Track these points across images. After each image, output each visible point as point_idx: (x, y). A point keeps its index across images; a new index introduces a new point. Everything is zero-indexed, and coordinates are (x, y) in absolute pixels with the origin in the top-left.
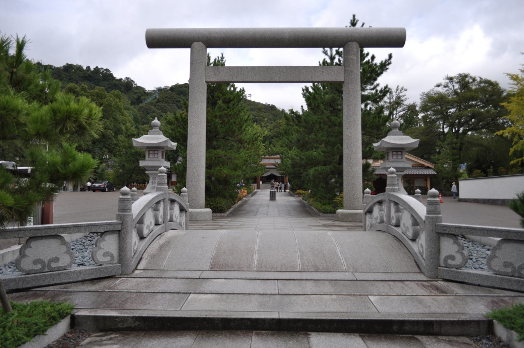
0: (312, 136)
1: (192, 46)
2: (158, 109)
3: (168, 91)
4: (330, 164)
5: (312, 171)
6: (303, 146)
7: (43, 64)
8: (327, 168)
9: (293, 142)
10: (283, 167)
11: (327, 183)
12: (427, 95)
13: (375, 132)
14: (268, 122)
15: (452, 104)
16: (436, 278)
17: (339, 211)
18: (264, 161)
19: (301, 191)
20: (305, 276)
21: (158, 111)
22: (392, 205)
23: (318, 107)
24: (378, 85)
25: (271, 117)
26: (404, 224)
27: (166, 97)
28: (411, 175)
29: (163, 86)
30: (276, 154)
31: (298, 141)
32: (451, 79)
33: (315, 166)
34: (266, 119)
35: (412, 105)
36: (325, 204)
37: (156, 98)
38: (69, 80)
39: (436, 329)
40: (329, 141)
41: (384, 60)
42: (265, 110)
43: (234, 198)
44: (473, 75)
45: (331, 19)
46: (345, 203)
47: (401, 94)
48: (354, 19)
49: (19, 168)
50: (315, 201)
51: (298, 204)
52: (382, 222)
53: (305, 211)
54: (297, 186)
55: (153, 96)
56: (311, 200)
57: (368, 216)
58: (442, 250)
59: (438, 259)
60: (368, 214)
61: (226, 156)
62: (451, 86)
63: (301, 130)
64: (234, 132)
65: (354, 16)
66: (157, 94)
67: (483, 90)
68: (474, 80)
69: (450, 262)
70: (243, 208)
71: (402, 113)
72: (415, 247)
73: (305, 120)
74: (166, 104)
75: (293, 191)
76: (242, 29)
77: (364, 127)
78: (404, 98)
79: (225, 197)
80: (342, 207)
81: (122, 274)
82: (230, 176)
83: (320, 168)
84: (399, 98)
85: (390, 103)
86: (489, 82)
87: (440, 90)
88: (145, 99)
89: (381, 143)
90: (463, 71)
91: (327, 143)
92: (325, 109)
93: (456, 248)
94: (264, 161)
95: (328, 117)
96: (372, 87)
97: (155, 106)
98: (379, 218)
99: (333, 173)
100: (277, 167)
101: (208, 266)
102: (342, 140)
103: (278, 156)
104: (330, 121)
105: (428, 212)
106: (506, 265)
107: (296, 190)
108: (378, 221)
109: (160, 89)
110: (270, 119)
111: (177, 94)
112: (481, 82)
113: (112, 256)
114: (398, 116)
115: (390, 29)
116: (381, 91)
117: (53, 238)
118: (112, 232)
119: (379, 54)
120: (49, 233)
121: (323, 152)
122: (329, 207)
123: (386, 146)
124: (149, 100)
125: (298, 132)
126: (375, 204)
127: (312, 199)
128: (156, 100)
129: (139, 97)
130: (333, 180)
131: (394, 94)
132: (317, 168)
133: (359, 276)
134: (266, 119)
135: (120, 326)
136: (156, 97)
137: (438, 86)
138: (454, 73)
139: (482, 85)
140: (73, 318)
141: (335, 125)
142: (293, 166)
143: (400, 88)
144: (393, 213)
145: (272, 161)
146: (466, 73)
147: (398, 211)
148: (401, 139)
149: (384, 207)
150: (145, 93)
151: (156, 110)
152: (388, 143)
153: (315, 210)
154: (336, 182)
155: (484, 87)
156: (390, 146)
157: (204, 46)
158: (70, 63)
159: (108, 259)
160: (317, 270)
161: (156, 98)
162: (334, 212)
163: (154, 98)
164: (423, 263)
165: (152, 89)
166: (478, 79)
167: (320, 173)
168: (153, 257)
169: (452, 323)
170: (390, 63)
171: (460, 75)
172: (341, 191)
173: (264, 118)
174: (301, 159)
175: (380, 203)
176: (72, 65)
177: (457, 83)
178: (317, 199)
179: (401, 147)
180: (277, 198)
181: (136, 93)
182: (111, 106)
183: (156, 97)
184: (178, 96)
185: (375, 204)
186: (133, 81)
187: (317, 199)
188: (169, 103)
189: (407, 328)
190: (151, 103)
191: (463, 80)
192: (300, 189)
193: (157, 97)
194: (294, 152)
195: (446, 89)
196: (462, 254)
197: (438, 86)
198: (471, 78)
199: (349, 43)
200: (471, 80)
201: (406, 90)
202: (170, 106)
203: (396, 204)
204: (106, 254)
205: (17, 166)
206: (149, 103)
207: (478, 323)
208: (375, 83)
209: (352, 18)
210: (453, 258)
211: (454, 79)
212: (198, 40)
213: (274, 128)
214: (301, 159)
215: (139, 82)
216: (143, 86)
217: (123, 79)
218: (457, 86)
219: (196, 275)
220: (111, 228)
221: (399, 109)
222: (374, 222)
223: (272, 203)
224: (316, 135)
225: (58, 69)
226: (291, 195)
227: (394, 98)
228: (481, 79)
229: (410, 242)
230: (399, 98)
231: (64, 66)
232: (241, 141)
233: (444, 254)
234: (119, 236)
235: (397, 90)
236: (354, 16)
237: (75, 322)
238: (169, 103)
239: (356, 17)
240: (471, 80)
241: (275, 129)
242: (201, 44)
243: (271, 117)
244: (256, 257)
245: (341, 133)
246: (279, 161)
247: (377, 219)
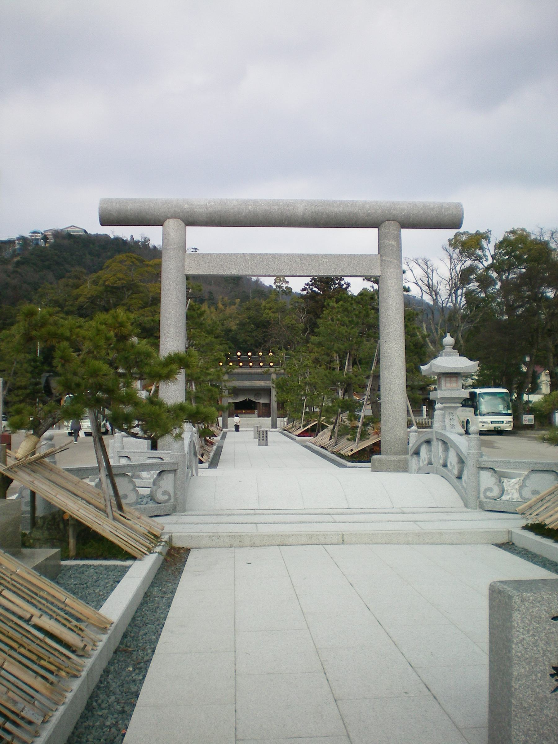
1: (166, 223)
22: (440, 443)
26: (451, 463)
58: (481, 484)
59: (479, 492)
60: (415, 456)
69: (489, 494)
89: (431, 366)
98: (427, 459)
106: (535, 492)
108: (426, 462)
113: (169, 495)
117: (122, 477)
118: (170, 471)
139: (212, 203)
152: (440, 366)
157: (183, 224)
159: (166, 497)
179: (456, 371)
203: (444, 443)
204: (165, 493)
210: (490, 489)
219: (252, 512)
222: (421, 465)
234: (175, 476)
247: (425, 460)
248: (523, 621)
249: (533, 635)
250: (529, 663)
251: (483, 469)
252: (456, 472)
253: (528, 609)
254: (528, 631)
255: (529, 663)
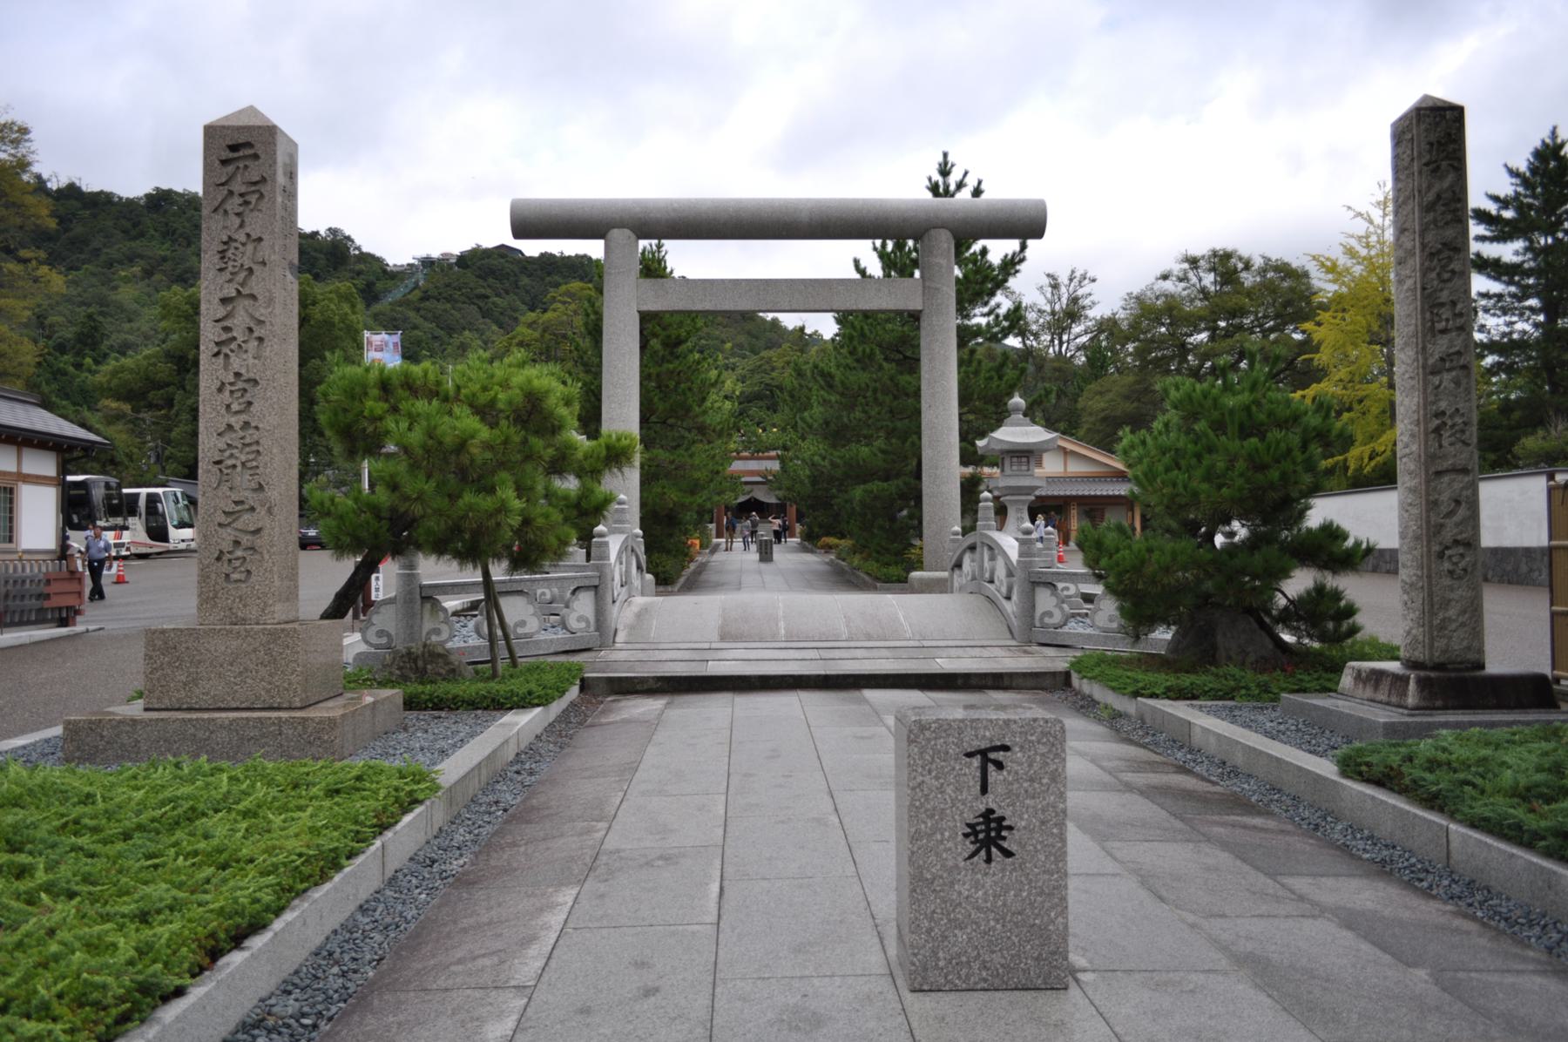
0: (858, 414)
2: (425, 319)
3: (450, 266)
4: (898, 476)
5: (858, 492)
6: (837, 434)
7: (84, 189)
8: (892, 486)
9: (815, 425)
10: (786, 483)
11: (893, 519)
12: (1137, 298)
13: (991, 408)
14: (733, 355)
15: (1194, 323)
16: (1030, 642)
17: (915, 574)
18: (737, 466)
19: (832, 540)
20: (852, 644)
21: (427, 325)
23: (871, 356)
24: (998, 306)
25: (742, 339)
27: (448, 285)
28: (1096, 497)
29: (435, 254)
30: (768, 449)
31: (827, 423)
32: (1193, 262)
33: (865, 482)
34: (728, 345)
35: (1109, 319)
36: (888, 564)
37: (416, 286)
38: (165, 235)
39: (1006, 682)
40: (894, 429)
41: (1010, 253)
42: (725, 321)
43: (685, 555)
44: (1244, 253)
45: (899, 183)
46: (927, 559)
47: (1080, 292)
48: (946, 163)
49: (125, 491)
50: (866, 560)
51: (827, 568)
52: (974, 578)
53: (845, 579)
54: (820, 526)
55: (410, 283)
56: (856, 560)
57: (957, 572)
59: (1032, 617)
61: (672, 462)
62: (1194, 280)
63: (833, 399)
64: (688, 410)
65: (945, 155)
66: (420, 276)
67: (1268, 288)
68: (1248, 266)
69: (1047, 620)
70: (704, 577)
71: (1084, 339)
72: (1010, 607)
73: (842, 383)
74: (448, 306)
75: (811, 540)
76: (712, 200)
77: (964, 400)
78: (1087, 302)
79: (668, 552)
80: (921, 569)
81: (602, 647)
82: (683, 505)
83: (876, 486)
84: (1074, 300)
85: (1053, 313)
86: (1284, 270)
87: (1169, 286)
88: (387, 291)
90: (1222, 244)
91: (890, 433)
92: (886, 359)
93: (1054, 600)
94: (737, 466)
95: (892, 379)
96: (986, 310)
97: (418, 310)
99: (903, 496)
100: (767, 481)
101: (716, 637)
102: (919, 427)
103: (773, 453)
104: (897, 385)
105: (1021, 555)
107: (818, 537)
109: (428, 262)
110: (740, 346)
111: (479, 277)
112: (1263, 272)
113: (588, 622)
114: (1072, 347)
115: (1014, 203)
116: (1006, 317)
118: (587, 588)
119: (998, 250)
120: (515, 587)
121: (883, 452)
122: (894, 571)
123: (998, 447)
124: (398, 293)
125: (825, 402)
126: (964, 552)
127: (858, 556)
128: (417, 293)
129: (370, 285)
130: (905, 513)
131: (1063, 290)
132: (869, 486)
133: (926, 643)
134: (728, 345)
135: (639, 687)
136: (417, 283)
137: (1165, 277)
138: (1200, 249)
139: (1270, 275)
140: (583, 680)
141: (907, 395)
142: (814, 480)
143: (1078, 274)
144: (987, 564)
145: (753, 465)
146: (1229, 248)
147: (992, 558)
148: (1027, 433)
149: (977, 555)
150: (385, 271)
151: (419, 321)
153: (867, 578)
154: (911, 517)
155: (1271, 281)
156: (1006, 447)
157: (633, 237)
158: (165, 187)
159: (583, 625)
160: (869, 638)
161: (416, 286)
162: (905, 580)
163: (411, 286)
164: (1015, 622)
165: (405, 263)
166: (1258, 262)
167: (876, 498)
168: (632, 628)
169: (1025, 675)
170: (1022, 260)
171: (1215, 254)
172: (920, 536)
173: (723, 342)
174: (833, 464)
175: (972, 548)
176: (169, 192)
177: (1210, 270)
178: (870, 555)
180: (776, 556)
181: (359, 273)
182: (333, 325)
183: (417, 283)
184: (481, 282)
185: (964, 552)
186: (348, 238)
187: (870, 555)
188: (456, 301)
189: (974, 682)
190: (404, 303)
191: (1224, 264)
192: (828, 534)
193: (421, 283)
194: (812, 448)
195: (1183, 285)
196: (1062, 609)
197: (1165, 277)
198: (1240, 259)
199: (933, 232)
200: (1240, 266)
201: (1094, 281)
202: (460, 310)
203: (990, 548)
204: (580, 619)
205: (120, 486)
206: (400, 303)
207: (1054, 674)
208: (993, 303)
209: (941, 159)
210: (1049, 614)
211: (1202, 263)
212: (620, 223)
213: (752, 371)
214: (833, 464)
215: (367, 240)
216: (378, 254)
217: (322, 233)
218: (1209, 279)
219: (706, 646)
220: (587, 583)
221: (1077, 329)
223: (763, 566)
224: (865, 412)
225: (131, 203)
226: (805, 550)
227: (1064, 300)
228: (1267, 260)
229: (1004, 602)
230: (1074, 300)
231: (147, 196)
232: (702, 429)
233: (1039, 611)
235: (1071, 280)
236: (945, 155)
237: (585, 685)
238: (456, 301)
239: (950, 159)
240: (1240, 266)
241: (757, 377)
242: (627, 232)
243: (742, 339)
244: (782, 624)
245: (918, 412)
246: (775, 466)
248: (921, 758)
249: (937, 778)
250: (932, 816)
251: (1038, 584)
252: (1004, 590)
253: (929, 740)
254: (930, 772)
255: (932, 816)
